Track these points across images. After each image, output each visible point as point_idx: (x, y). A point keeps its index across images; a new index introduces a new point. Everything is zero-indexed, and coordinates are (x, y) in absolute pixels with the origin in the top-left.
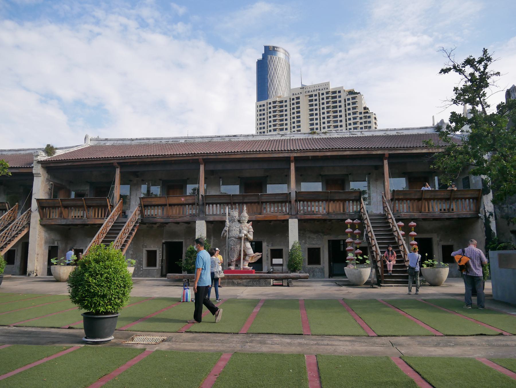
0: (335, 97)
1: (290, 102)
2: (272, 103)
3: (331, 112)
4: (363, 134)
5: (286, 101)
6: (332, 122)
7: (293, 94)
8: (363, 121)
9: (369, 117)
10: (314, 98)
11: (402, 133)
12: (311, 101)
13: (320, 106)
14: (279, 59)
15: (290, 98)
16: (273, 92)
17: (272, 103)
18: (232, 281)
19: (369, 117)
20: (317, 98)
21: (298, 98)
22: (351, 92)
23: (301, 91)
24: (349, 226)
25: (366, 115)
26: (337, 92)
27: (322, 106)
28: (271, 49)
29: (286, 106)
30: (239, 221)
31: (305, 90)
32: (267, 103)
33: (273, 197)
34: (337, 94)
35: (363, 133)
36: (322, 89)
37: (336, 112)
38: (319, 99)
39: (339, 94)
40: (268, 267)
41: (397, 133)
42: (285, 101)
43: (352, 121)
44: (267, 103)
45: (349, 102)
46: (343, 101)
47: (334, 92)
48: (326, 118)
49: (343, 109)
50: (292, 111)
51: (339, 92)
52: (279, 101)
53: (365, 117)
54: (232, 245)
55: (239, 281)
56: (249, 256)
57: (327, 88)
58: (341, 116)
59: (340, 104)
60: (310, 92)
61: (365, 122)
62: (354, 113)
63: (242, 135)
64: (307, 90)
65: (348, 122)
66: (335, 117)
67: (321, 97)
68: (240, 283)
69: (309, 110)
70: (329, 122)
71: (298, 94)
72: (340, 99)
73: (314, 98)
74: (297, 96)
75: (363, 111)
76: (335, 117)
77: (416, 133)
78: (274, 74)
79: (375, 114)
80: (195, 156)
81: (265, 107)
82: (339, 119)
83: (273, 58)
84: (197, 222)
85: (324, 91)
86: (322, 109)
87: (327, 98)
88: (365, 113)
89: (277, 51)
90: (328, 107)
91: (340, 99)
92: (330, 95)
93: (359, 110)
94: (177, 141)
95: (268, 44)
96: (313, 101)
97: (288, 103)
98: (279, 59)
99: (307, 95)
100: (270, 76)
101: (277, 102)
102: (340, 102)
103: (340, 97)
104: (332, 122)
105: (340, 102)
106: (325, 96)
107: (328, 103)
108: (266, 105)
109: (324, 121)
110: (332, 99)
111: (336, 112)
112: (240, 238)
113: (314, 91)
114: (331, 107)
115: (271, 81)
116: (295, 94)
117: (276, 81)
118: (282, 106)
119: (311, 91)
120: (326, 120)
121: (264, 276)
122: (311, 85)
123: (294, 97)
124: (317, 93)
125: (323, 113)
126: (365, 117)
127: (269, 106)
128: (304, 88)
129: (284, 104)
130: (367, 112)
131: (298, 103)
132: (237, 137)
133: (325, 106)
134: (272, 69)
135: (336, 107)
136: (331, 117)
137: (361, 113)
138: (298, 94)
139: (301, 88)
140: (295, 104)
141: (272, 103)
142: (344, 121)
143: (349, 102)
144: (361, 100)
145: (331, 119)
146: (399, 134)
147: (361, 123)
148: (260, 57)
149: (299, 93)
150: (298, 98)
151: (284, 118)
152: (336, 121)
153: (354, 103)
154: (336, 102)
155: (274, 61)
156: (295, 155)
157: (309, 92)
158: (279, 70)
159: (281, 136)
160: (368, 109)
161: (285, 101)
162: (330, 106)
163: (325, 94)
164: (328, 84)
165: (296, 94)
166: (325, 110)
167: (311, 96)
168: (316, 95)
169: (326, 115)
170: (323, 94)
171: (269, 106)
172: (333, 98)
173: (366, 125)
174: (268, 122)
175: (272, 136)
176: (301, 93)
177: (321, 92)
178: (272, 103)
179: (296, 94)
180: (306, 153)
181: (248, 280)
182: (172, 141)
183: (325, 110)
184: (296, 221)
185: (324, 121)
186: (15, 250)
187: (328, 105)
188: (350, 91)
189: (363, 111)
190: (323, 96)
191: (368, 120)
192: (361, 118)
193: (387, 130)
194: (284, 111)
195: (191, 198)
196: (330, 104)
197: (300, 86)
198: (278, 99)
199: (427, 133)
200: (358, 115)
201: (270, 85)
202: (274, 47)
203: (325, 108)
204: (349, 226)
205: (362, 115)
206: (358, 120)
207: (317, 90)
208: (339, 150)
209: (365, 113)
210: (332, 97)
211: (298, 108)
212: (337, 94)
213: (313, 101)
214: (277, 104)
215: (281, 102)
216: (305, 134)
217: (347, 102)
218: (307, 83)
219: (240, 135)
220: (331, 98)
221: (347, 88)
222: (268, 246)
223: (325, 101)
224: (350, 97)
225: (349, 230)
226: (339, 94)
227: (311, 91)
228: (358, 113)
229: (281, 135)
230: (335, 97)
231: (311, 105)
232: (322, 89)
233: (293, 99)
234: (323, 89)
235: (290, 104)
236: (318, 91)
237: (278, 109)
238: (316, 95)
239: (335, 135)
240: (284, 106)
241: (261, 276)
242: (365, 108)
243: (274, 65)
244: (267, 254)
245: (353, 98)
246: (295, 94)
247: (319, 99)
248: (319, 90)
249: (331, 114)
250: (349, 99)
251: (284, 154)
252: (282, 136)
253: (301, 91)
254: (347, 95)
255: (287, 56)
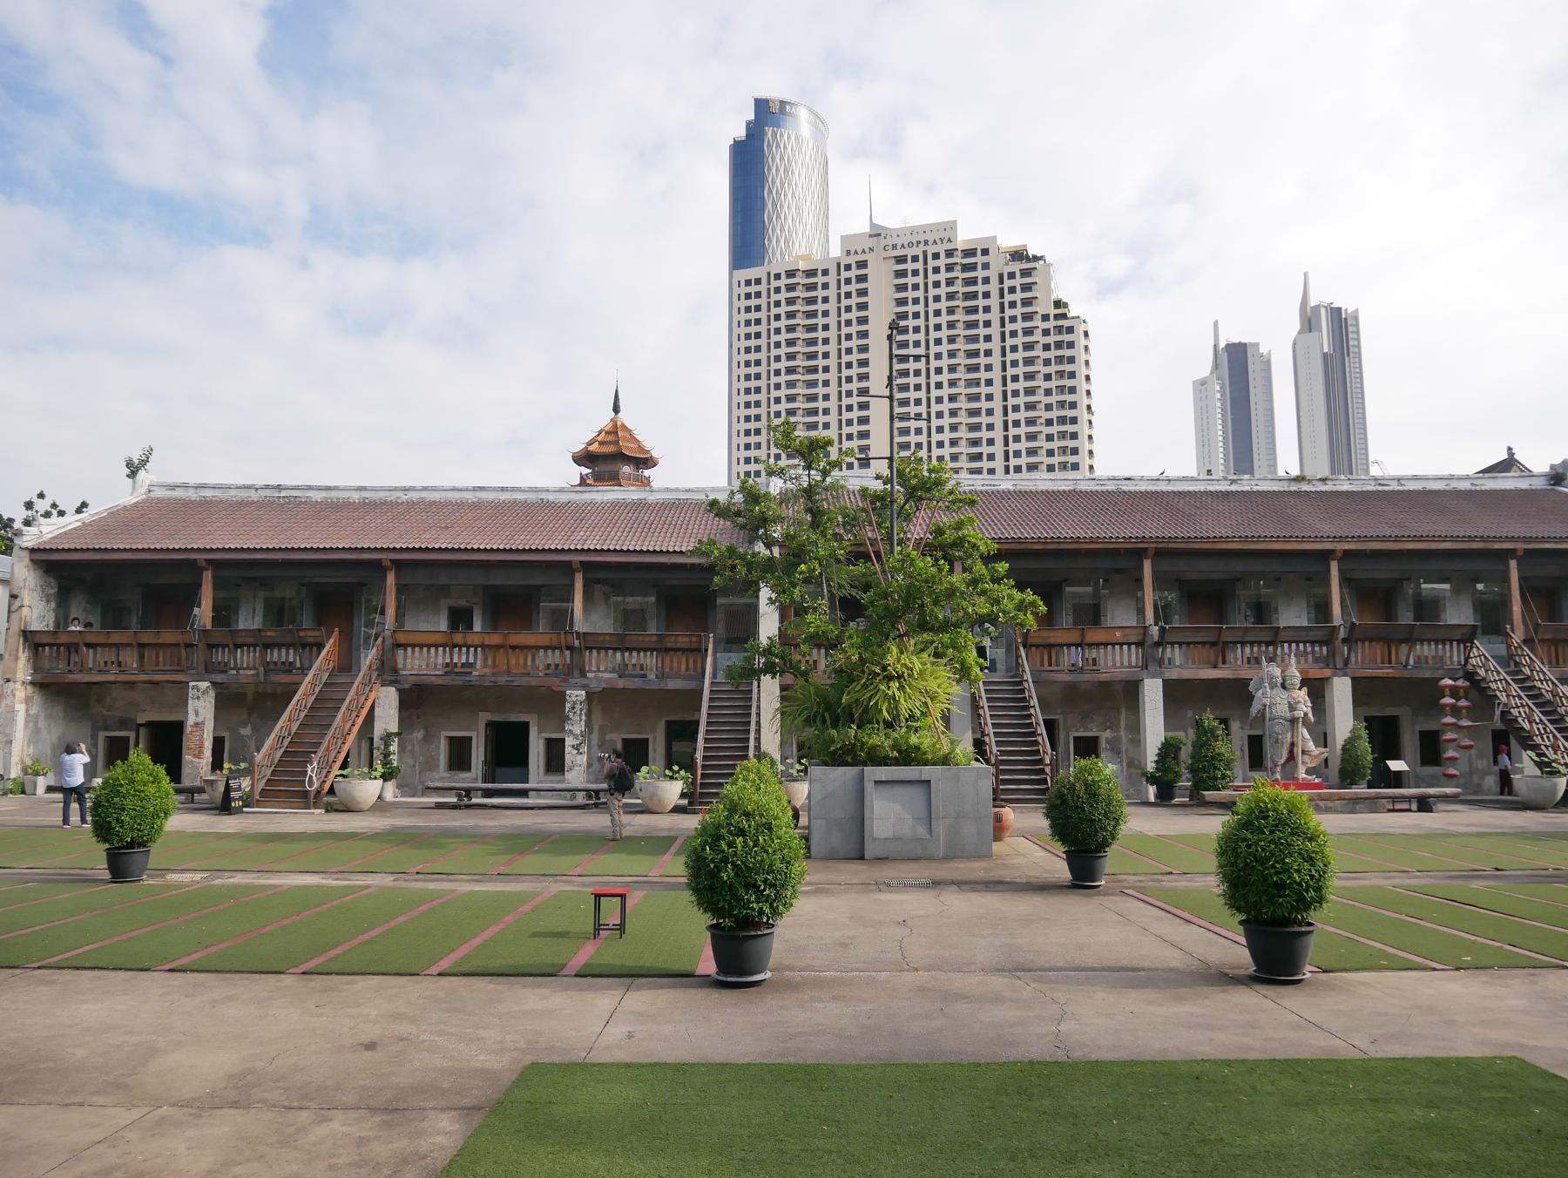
0: (973, 267)
1: (839, 274)
2: (783, 276)
3: (960, 310)
4: (1402, 485)
5: (825, 272)
6: (961, 339)
7: (848, 253)
8: (1051, 339)
9: (1070, 330)
10: (910, 266)
11: (1482, 485)
12: (901, 274)
13: (926, 291)
14: (797, 138)
15: (839, 265)
16: (778, 241)
17: (783, 276)
18: (1316, 804)
19: (1070, 330)
20: (919, 265)
21: (862, 264)
22: (1018, 255)
23: (872, 242)
24: (1447, 691)
25: (1060, 323)
26: (979, 252)
27: (932, 292)
28: (775, 108)
29: (825, 286)
30: (1284, 686)
31: (883, 242)
32: (769, 274)
33: (1304, 633)
34: (979, 259)
35: (1402, 482)
36: (935, 242)
37: (974, 310)
38: (926, 271)
39: (984, 259)
40: (1244, 772)
41: (1472, 484)
42: (982, 250)
43: (1020, 340)
44: (769, 274)
45: (1012, 283)
46: (994, 280)
47: (970, 253)
48: (944, 326)
49: (994, 302)
50: (845, 302)
51: (985, 252)
52: (803, 271)
53: (1059, 329)
54: (1278, 734)
55: (1329, 804)
56: (1310, 755)
57: (949, 240)
58: (987, 324)
59: (986, 288)
60: (899, 247)
61: (1059, 345)
62: (1027, 317)
63: (1145, 478)
64: (890, 242)
65: (1010, 342)
66: (972, 325)
67: (931, 263)
68: (1331, 808)
69: (894, 303)
70: (952, 340)
71: (864, 251)
72: (985, 273)
73: (910, 266)
74: (861, 258)
75: (1053, 311)
76: (972, 325)
77: (1512, 487)
78: (782, 185)
79: (1084, 321)
80: (1142, 542)
81: (763, 288)
82: (982, 331)
83: (781, 135)
84: (1145, 680)
85: (941, 249)
86: (934, 301)
87: (949, 268)
88: (1057, 317)
89: (790, 115)
90: (950, 296)
91: (985, 273)
92: (958, 260)
93: (1040, 308)
94: (994, 485)
95: (763, 95)
96: (906, 276)
97: (831, 279)
98: (797, 138)
99: (890, 258)
100: (770, 192)
101: (800, 287)
102: (986, 281)
103: (986, 266)
104: (961, 339)
105: (986, 281)
106: (942, 262)
107: (950, 282)
108: (764, 281)
109: (938, 335)
110: (963, 271)
111: (974, 310)
112: (1293, 721)
113: (911, 245)
114: (960, 295)
115: (774, 205)
116: (852, 252)
117: (788, 207)
118: (812, 287)
119: (903, 246)
120: (944, 333)
121: (1385, 793)
122: (903, 226)
123: (852, 260)
124: (918, 251)
125: (937, 313)
126: (1059, 329)
127: (774, 284)
128: (880, 235)
129: (820, 279)
130: (1064, 316)
131: (862, 279)
132: (1132, 482)
133: (943, 291)
134: (777, 170)
135: (974, 296)
136: (960, 325)
137: (1045, 318)
138: (864, 251)
139: (870, 236)
140: (854, 280)
141: (783, 276)
142: (996, 338)
143: (1012, 283)
144: (1048, 278)
145: (960, 331)
146: (1478, 488)
147: (1047, 347)
148: (741, 133)
149: (867, 250)
150: (862, 264)
151: (820, 321)
152: (974, 339)
153: (1027, 288)
154: (973, 281)
155: (782, 146)
156: (1346, 547)
157: (894, 247)
158: (797, 173)
159: (1229, 482)
160: (1066, 305)
161: (982, 250)
162: (958, 292)
163: (943, 255)
164: (951, 226)
165: (856, 252)
166: (943, 305)
167: (901, 260)
168: (915, 259)
169: (944, 319)
170: (936, 256)
171: (774, 284)
172: (966, 268)
173: (1060, 353)
174: (772, 331)
175: (1210, 482)
176: (871, 249)
177: (931, 250)
178: (783, 276)
179: (856, 252)
180: (1366, 543)
181: (1346, 802)
182: (983, 485)
183: (943, 305)
184: (1348, 681)
185: (938, 335)
186: (647, 740)
187: (951, 289)
188: (1016, 252)
189: (1053, 311)
190: (936, 263)
191: (1067, 338)
192: (1046, 332)
193: (1451, 478)
194: (820, 300)
195: (1135, 632)
196: (958, 287)
197: (867, 229)
198: (802, 266)
199: (1533, 487)
200: (1037, 322)
201: (770, 219)
202: (783, 103)
203: (943, 297)
204: (1447, 691)
205: (1051, 324)
206: (1037, 336)
207: (919, 242)
208: (1432, 539)
209: (1057, 317)
210: (963, 265)
211: (863, 293)
212: (979, 259)
213: (906, 276)
214: (800, 279)
215: (811, 273)
216: (1280, 480)
217: (1008, 283)
218: (891, 220)
219: (1139, 478)
220: (959, 268)
221: (1008, 241)
222: (1242, 728)
223: (943, 276)
224: (1016, 267)
225: (1448, 700)
226: (984, 259)
227: (903, 246)
228: (1039, 317)
229: (1229, 482)
230: (973, 267)
231: (902, 288)
232: (935, 242)
233: (848, 267)
234: (939, 242)
235: (839, 281)
236: (922, 247)
237: (800, 293)
238: (915, 259)
239: (1346, 487)
240: (820, 286)
241: (1380, 793)
242: (1058, 304)
243: (782, 158)
244: (1242, 746)
245: (1026, 273)
246: (852, 252)
247: (926, 271)
248: (926, 243)
249: (960, 316)
250: (1012, 276)
251: (1325, 544)
252: (1231, 483)
253: (872, 242)
254: (1007, 264)
255: (820, 131)
